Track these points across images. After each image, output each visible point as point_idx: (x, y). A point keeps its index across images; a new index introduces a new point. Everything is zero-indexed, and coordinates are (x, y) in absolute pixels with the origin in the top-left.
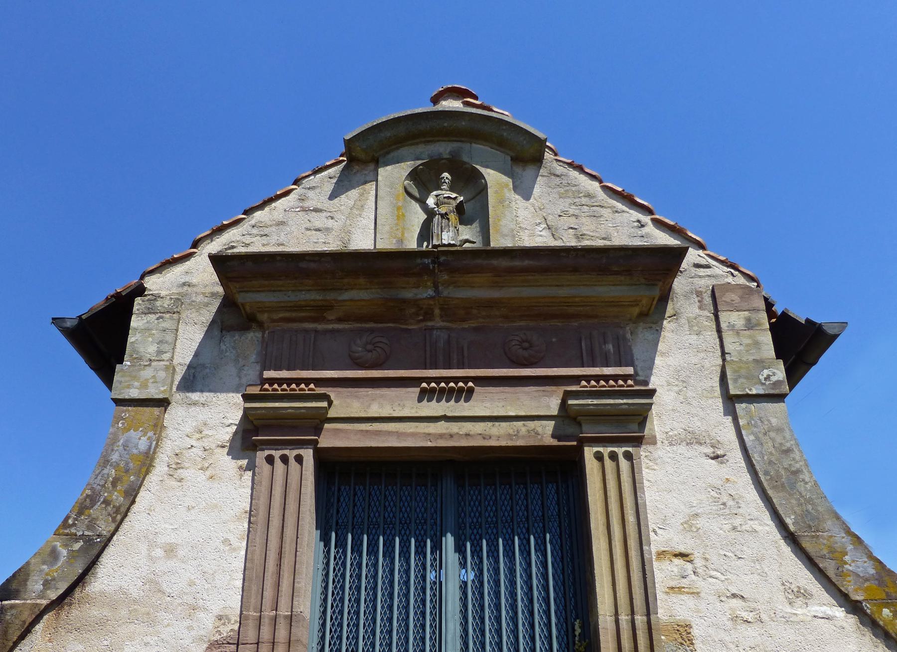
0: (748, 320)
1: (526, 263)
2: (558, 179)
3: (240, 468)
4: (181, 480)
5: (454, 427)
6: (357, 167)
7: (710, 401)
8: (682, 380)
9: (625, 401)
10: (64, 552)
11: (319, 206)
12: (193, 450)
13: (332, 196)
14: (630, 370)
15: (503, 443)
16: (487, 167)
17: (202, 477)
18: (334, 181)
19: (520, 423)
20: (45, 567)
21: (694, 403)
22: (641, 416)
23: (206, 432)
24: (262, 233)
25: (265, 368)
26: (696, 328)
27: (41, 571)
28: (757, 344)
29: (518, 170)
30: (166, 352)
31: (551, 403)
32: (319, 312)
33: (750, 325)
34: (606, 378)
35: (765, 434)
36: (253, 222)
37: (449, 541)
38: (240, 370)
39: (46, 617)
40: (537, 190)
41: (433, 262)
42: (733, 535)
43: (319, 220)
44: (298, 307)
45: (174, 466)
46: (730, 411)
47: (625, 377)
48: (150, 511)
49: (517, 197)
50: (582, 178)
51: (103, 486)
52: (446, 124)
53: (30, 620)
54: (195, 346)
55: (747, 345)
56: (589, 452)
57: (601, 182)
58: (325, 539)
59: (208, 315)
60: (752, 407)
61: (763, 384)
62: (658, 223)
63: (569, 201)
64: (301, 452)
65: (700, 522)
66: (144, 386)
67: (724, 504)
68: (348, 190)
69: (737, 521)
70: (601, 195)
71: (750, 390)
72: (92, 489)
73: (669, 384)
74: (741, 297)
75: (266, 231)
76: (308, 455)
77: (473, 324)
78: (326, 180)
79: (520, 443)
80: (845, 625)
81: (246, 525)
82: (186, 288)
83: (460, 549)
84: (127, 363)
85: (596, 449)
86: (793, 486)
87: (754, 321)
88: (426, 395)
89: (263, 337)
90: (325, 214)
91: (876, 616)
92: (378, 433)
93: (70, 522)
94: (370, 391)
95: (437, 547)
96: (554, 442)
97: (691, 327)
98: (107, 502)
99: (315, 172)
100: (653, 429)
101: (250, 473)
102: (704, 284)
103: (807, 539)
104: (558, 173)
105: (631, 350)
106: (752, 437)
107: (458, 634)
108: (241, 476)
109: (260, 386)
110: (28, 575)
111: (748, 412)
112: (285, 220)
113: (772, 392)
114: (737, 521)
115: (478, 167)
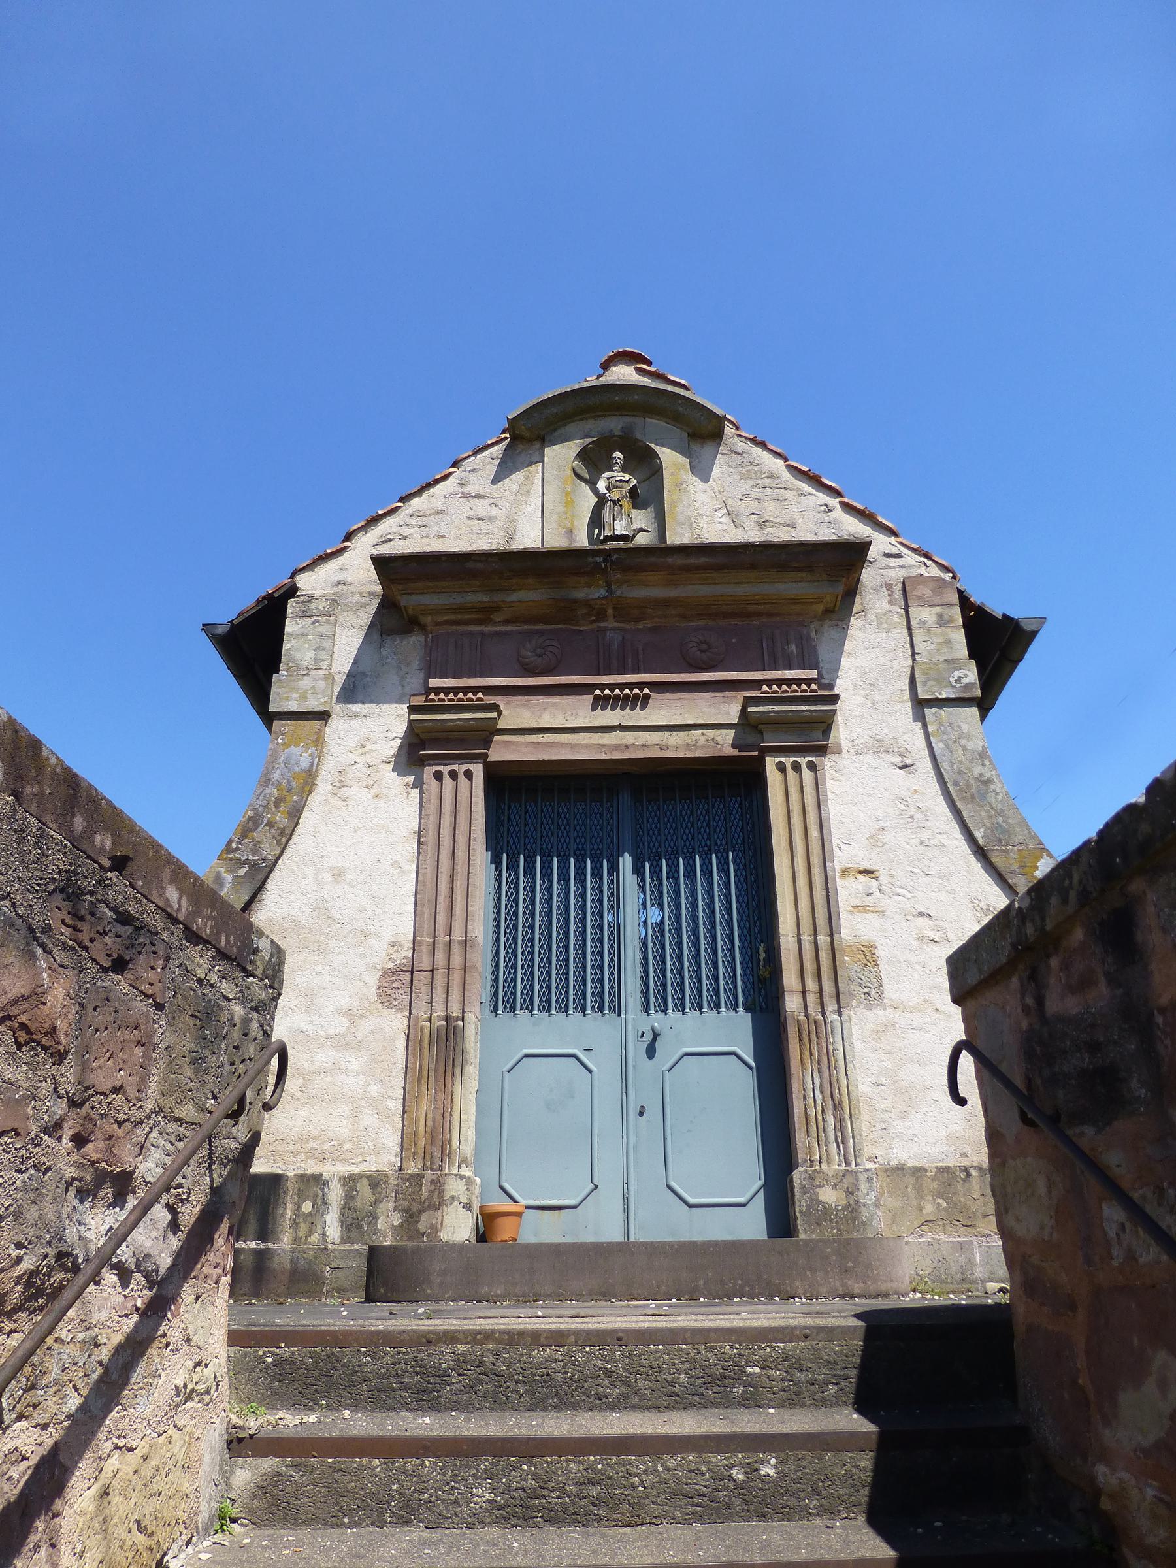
0: (940, 616)
1: (703, 560)
2: (739, 457)
3: (407, 785)
5: (630, 738)
6: (521, 446)
7: (899, 706)
9: (807, 707)
11: (481, 492)
12: (357, 766)
13: (496, 480)
14: (813, 673)
15: (681, 755)
16: (662, 445)
17: (367, 795)
21: (882, 708)
22: (825, 724)
24: (421, 523)
25: (429, 676)
28: (948, 643)
29: (695, 447)
30: (323, 660)
31: (729, 709)
32: (486, 613)
33: (942, 622)
35: (955, 741)
36: (410, 511)
38: (403, 678)
40: (717, 470)
41: (605, 561)
42: (921, 849)
45: (337, 784)
46: (920, 717)
47: (808, 682)
49: (695, 478)
50: (766, 455)
51: (266, 807)
55: (939, 644)
56: (771, 763)
57: (786, 460)
58: (496, 861)
59: (366, 617)
60: (942, 711)
61: (955, 687)
62: (847, 507)
63: (751, 482)
65: (887, 837)
66: (303, 697)
67: (912, 817)
68: (512, 473)
69: (925, 836)
70: (786, 475)
71: (940, 693)
73: (856, 688)
75: (425, 521)
76: (478, 769)
77: (648, 624)
79: (699, 753)
81: (415, 847)
82: (341, 587)
83: (638, 870)
85: (778, 760)
86: (983, 796)
87: (946, 617)
88: (600, 703)
89: (426, 640)
90: (487, 501)
92: (550, 745)
93: (234, 846)
94: (541, 700)
95: (614, 868)
96: (735, 753)
97: (880, 624)
98: (270, 824)
101: (417, 791)
105: (816, 651)
107: (638, 961)
108: (408, 793)
113: (962, 695)
114: (925, 836)
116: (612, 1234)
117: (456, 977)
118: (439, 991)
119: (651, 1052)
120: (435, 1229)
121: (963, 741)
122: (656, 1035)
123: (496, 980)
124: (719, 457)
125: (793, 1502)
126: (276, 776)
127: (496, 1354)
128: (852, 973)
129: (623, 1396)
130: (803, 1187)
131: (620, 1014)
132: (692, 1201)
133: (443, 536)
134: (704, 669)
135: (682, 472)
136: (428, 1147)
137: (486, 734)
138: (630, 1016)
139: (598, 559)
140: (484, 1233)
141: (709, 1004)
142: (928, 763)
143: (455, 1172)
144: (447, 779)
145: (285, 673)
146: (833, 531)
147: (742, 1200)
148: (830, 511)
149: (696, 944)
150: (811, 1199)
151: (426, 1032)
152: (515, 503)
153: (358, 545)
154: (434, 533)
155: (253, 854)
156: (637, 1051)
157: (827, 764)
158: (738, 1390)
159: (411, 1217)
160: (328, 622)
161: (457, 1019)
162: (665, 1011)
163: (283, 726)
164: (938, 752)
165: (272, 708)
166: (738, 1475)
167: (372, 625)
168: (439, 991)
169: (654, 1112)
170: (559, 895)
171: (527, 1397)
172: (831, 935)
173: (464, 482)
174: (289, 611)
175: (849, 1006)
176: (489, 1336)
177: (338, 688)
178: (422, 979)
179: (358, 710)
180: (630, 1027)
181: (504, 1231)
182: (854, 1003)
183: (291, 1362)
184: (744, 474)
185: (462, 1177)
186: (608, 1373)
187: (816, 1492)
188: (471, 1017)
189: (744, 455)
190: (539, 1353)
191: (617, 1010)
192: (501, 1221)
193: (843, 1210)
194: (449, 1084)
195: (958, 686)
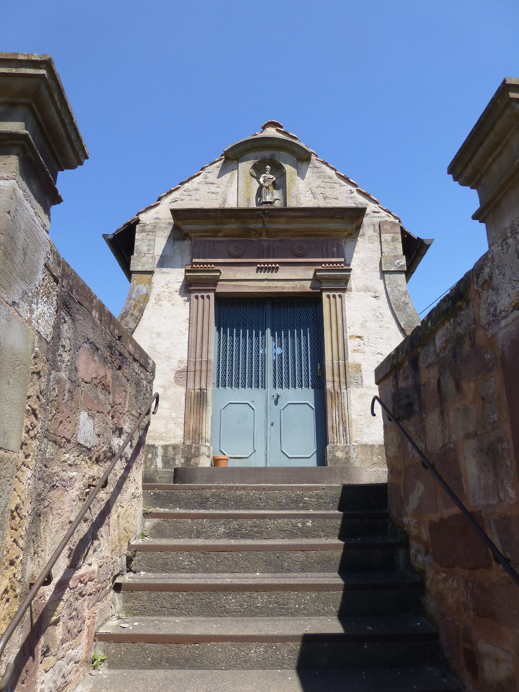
0: (393, 237)
1: (301, 214)
3: (185, 300)
4: (161, 306)
5: (271, 284)
9: (339, 273)
14: (342, 260)
15: (290, 291)
16: (286, 163)
17: (169, 304)
18: (219, 169)
19: (297, 282)
21: (368, 274)
22: (346, 280)
24: (189, 194)
25: (193, 257)
28: (396, 248)
29: (300, 164)
30: (151, 250)
31: (309, 273)
32: (215, 233)
33: (394, 240)
34: (333, 263)
35: (396, 287)
36: (184, 189)
37: (268, 331)
40: (308, 175)
41: (263, 213)
43: (213, 188)
45: (157, 300)
46: (383, 278)
47: (340, 263)
49: (299, 178)
50: (328, 169)
51: (130, 308)
55: (392, 249)
56: (324, 295)
57: (336, 171)
58: (219, 330)
59: (167, 232)
62: (359, 192)
63: (321, 180)
64: (209, 294)
65: (367, 324)
66: (144, 265)
69: (382, 324)
70: (335, 177)
72: (126, 309)
74: (391, 227)
75: (190, 193)
76: (212, 295)
79: (297, 290)
82: (157, 220)
84: (135, 255)
85: (327, 293)
87: (395, 238)
88: (259, 270)
90: (215, 185)
92: (240, 286)
94: (237, 268)
95: (264, 334)
96: (311, 290)
97: (369, 240)
98: (132, 315)
99: (211, 164)
100: (351, 285)
101: (188, 303)
102: (377, 220)
104: (317, 166)
105: (344, 250)
106: (390, 289)
107: (272, 369)
108: (185, 304)
111: (390, 278)
113: (399, 269)
114: (382, 324)
117: (204, 374)
118: (197, 379)
119: (276, 403)
120: (197, 464)
121: (398, 288)
122: (278, 397)
123: (219, 375)
125: (316, 533)
126: (134, 296)
127: (224, 493)
128: (352, 375)
129: (264, 506)
130: (330, 451)
131: (265, 389)
132: (290, 456)
133: (198, 200)
136: (194, 436)
137: (215, 281)
138: (269, 389)
139: (260, 213)
141: (298, 385)
142: (384, 296)
144: (200, 299)
145: (136, 255)
147: (308, 456)
148: (352, 193)
151: (193, 394)
152: (227, 187)
154: (194, 198)
156: (271, 402)
157: (346, 295)
158: (301, 505)
160: (153, 235)
161: (204, 389)
162: (282, 388)
163: (135, 276)
166: (300, 525)
167: (170, 236)
168: (197, 379)
169: (277, 425)
172: (345, 361)
174: (137, 230)
178: (191, 374)
180: (268, 393)
181: (222, 464)
182: (352, 386)
183: (159, 494)
185: (206, 446)
186: (260, 499)
187: (323, 531)
188: (210, 389)
190: (238, 493)
191: (264, 387)
194: (201, 413)
195: (398, 266)
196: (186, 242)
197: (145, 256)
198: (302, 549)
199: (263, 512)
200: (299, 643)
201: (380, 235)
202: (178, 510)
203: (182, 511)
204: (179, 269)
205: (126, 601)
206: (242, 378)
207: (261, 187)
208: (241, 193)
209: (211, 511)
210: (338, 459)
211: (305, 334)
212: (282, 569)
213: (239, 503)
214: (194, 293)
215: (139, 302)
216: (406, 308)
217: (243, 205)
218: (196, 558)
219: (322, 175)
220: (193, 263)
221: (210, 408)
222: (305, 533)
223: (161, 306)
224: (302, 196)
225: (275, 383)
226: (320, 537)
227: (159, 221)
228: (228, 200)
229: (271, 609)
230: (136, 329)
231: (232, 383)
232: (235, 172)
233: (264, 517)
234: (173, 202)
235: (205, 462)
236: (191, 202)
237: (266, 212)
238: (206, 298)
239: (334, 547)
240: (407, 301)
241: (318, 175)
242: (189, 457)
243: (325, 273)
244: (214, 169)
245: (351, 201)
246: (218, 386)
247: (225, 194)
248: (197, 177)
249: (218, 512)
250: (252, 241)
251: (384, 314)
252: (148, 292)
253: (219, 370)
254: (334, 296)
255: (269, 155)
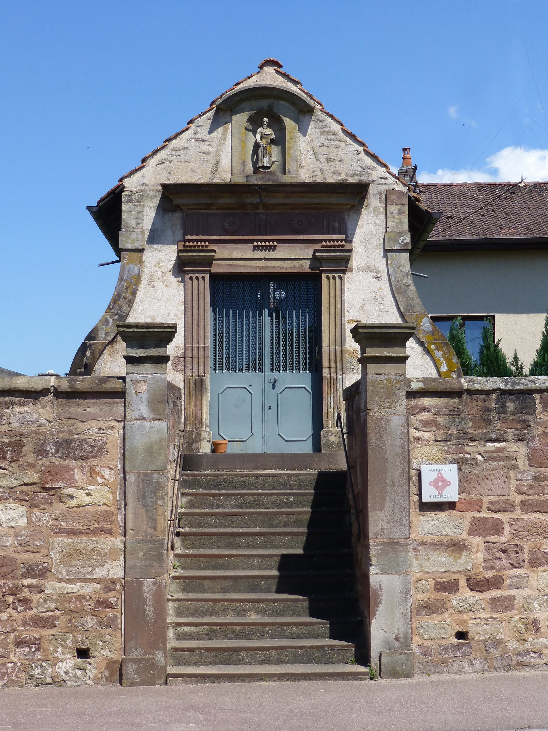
0: (399, 210)
1: (300, 189)
2: (321, 123)
3: (178, 281)
4: (154, 287)
5: (268, 263)
6: (221, 113)
7: (378, 251)
8: (366, 242)
9: (339, 254)
10: (111, 320)
11: (204, 138)
12: (157, 273)
13: (210, 132)
14: (344, 237)
15: (289, 271)
16: (286, 116)
17: (162, 286)
18: (211, 121)
19: (296, 261)
20: (104, 327)
21: (371, 252)
22: (347, 260)
23: (162, 264)
24: (177, 154)
25: (185, 234)
26: (376, 213)
27: (103, 328)
28: (401, 223)
29: (301, 117)
30: (140, 224)
31: (309, 253)
32: (208, 206)
33: (400, 212)
34: (334, 240)
35: (398, 268)
36: (172, 147)
37: (266, 312)
38: (174, 233)
39: (107, 347)
40: (310, 130)
41: (259, 188)
42: (380, 312)
43: (204, 147)
44: (198, 205)
45: (150, 281)
46: (385, 256)
47: (342, 240)
48: (143, 301)
49: (300, 134)
50: (333, 122)
51: (122, 290)
52: (266, 93)
53: (102, 349)
54: (152, 220)
55: (397, 223)
56: (324, 276)
57: (342, 125)
58: (214, 311)
59: (156, 202)
60: (394, 254)
61: (400, 244)
62: (367, 153)
63: (325, 137)
64: (204, 275)
65: (367, 307)
66: (133, 242)
67: (377, 299)
68: (218, 128)
69: (381, 307)
70: (341, 134)
71: (394, 247)
72: (118, 292)
73: (361, 242)
74: (398, 198)
75: (179, 153)
76: (207, 276)
77: (277, 211)
78: (206, 120)
79: (296, 271)
80: (417, 351)
81: (183, 308)
82: (144, 187)
83: (271, 315)
84: (123, 230)
85: (327, 274)
86: (406, 291)
87: (402, 210)
88: (256, 248)
89: (183, 215)
90: (207, 143)
91: (428, 348)
92: (236, 266)
93: (111, 307)
94: (232, 246)
95: (261, 314)
96: (310, 271)
97: (374, 212)
98: (125, 298)
99: (200, 116)
100: (352, 265)
101: (182, 284)
102: (384, 188)
103: (408, 315)
104: (321, 119)
105: (346, 225)
106: (392, 269)
107: (270, 352)
108: (179, 285)
109: (183, 243)
110: (98, 330)
111: (392, 257)
112: (188, 146)
113: (403, 248)
114: (381, 307)
115: (281, 116)
116: (259, 451)
117: (202, 360)
118: (195, 365)
119: (274, 387)
120: (198, 449)
121: (401, 268)
122: (275, 381)
123: (215, 359)
124: (312, 122)
125: (296, 505)
126: (125, 277)
127: (233, 478)
128: (348, 361)
129: (262, 487)
130: (324, 436)
131: (262, 373)
132: (287, 439)
133: (187, 162)
134: (298, 233)
135: (294, 131)
136: (194, 421)
137: (209, 262)
138: (266, 373)
139: (256, 188)
140: (214, 449)
141: (296, 369)
142: (386, 276)
143: (204, 430)
144: (195, 280)
145: (124, 230)
146: (359, 164)
147: (304, 439)
148: (359, 154)
149: (292, 345)
150: (327, 440)
151: (191, 380)
152: (220, 145)
153: (149, 164)
154: (183, 160)
155: (119, 310)
156: (268, 386)
157: (347, 276)
158: (288, 486)
159: (189, 445)
160: (140, 205)
161: (203, 376)
162: (279, 371)
163: (126, 254)
164: (390, 272)
165: (121, 247)
166: (285, 500)
167: (159, 206)
168: (195, 365)
169: (274, 408)
170: (239, 325)
171: (240, 487)
172: (342, 346)
173: (196, 132)
174: (123, 199)
175: (346, 373)
176: (231, 475)
177: (146, 237)
178: (189, 361)
179: (156, 247)
180: (266, 377)
181: (221, 449)
182: (348, 372)
183: (186, 480)
184: (322, 133)
185: (207, 432)
186: (258, 483)
187: (301, 503)
188: (208, 376)
189: (323, 122)
190: (243, 478)
191: (261, 370)
192: (220, 446)
193: (337, 443)
194: (200, 399)
195: (402, 243)
196: (177, 213)
197: (133, 231)
198: (285, 514)
199: (260, 491)
200: (279, 558)
201: (386, 207)
202: (201, 491)
203: (203, 491)
204: (171, 246)
205: (183, 541)
206: (239, 361)
207: (257, 146)
208: (236, 154)
209: (224, 491)
210: (332, 443)
211: (304, 315)
212: (273, 525)
213: (243, 486)
214: (188, 274)
215: (131, 283)
216: (407, 291)
217: (241, 180)
218: (219, 520)
219: (326, 132)
220: (185, 241)
221: (208, 394)
222: (289, 505)
223: (154, 287)
224: (303, 157)
225: (273, 367)
226: (299, 507)
227: (146, 188)
228: (221, 163)
229: (265, 545)
230: (130, 313)
231: (229, 367)
232: (229, 125)
233: (261, 494)
234: (160, 164)
235: (206, 448)
236: (180, 163)
237: (263, 187)
238: (201, 279)
239: (306, 513)
240: (409, 283)
241: (322, 130)
242: (191, 441)
243: (325, 254)
244: (205, 121)
245: (357, 164)
246: (215, 370)
247: (218, 154)
248: (186, 132)
249: (229, 492)
250: (248, 213)
251: (385, 296)
252: (139, 272)
253: (215, 353)
254: (334, 278)
255: (267, 105)
